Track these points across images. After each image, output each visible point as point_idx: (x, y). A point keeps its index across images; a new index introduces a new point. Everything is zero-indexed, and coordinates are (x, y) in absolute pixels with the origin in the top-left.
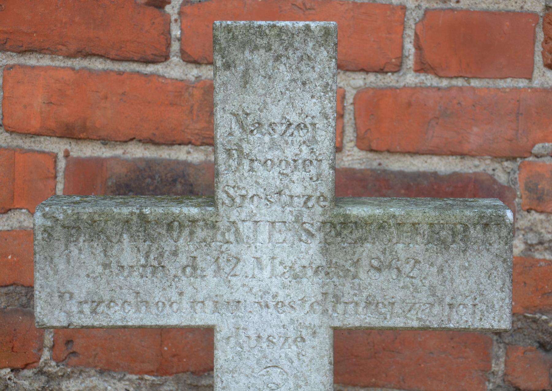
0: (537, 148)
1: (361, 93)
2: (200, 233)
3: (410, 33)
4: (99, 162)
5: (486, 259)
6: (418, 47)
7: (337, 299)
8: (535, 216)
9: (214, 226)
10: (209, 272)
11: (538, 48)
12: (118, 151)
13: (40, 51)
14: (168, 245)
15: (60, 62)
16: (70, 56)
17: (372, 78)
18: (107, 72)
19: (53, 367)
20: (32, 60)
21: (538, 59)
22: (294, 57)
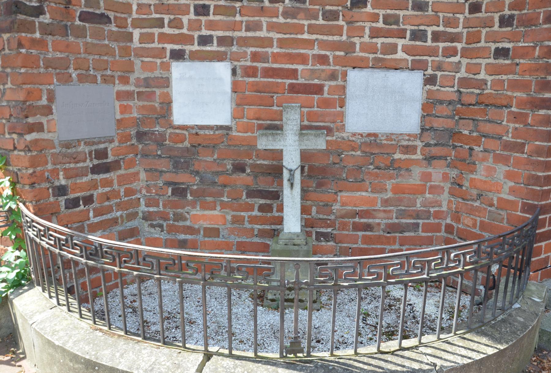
0: (338, 121)
1: (307, 112)
2: (281, 135)
3: (316, 101)
4: (262, 124)
5: (322, 139)
6: (317, 104)
7: (301, 145)
8: (338, 133)
9: (283, 134)
10: (282, 141)
11: (338, 104)
12: (265, 122)
13: (253, 105)
14: (276, 137)
15: (256, 107)
16: (257, 106)
17: (309, 109)
18: (263, 109)
19: (255, 159)
20: (251, 107)
21: (338, 106)
22: (294, 109)
